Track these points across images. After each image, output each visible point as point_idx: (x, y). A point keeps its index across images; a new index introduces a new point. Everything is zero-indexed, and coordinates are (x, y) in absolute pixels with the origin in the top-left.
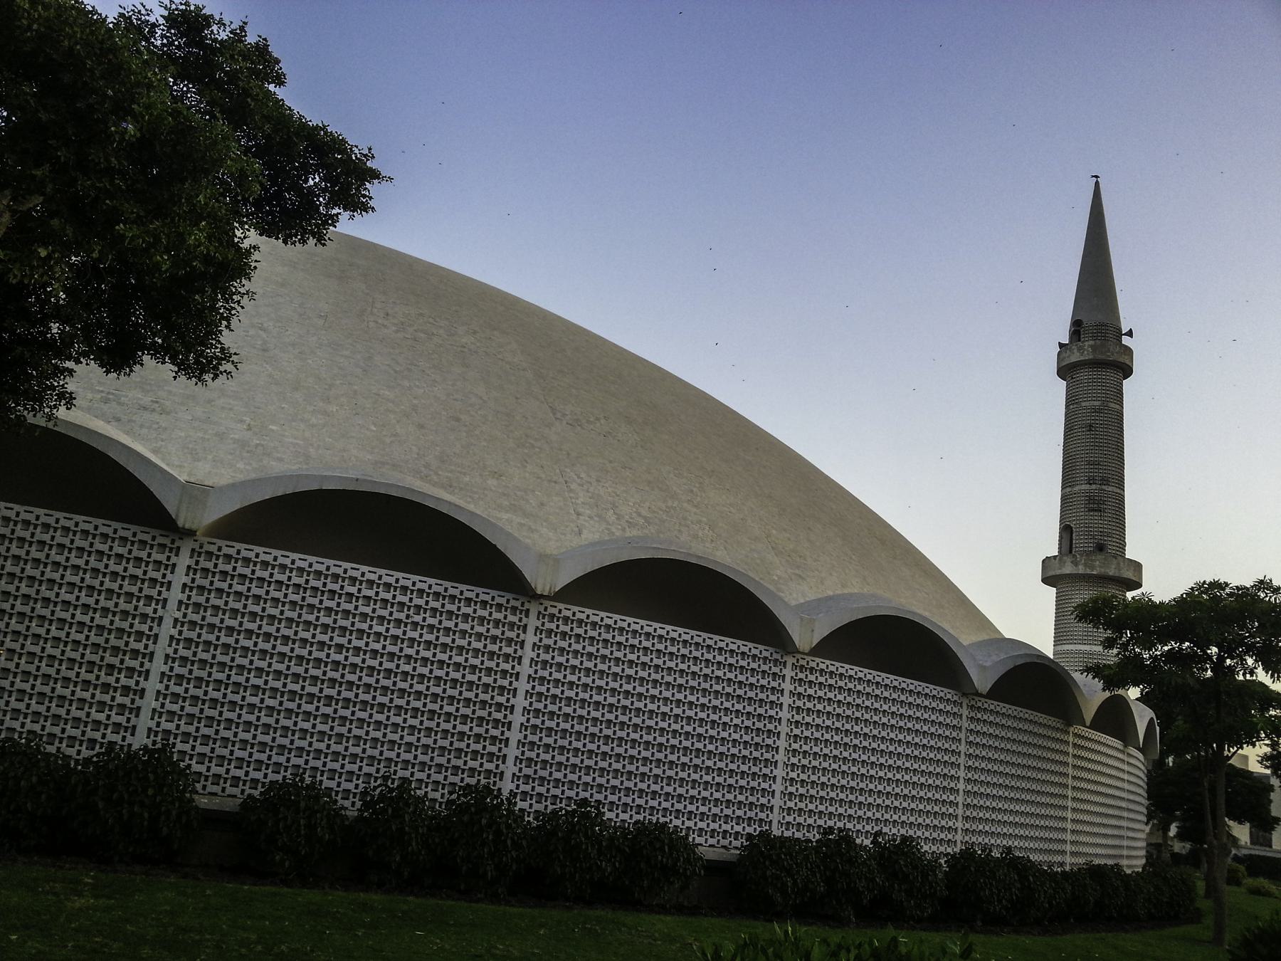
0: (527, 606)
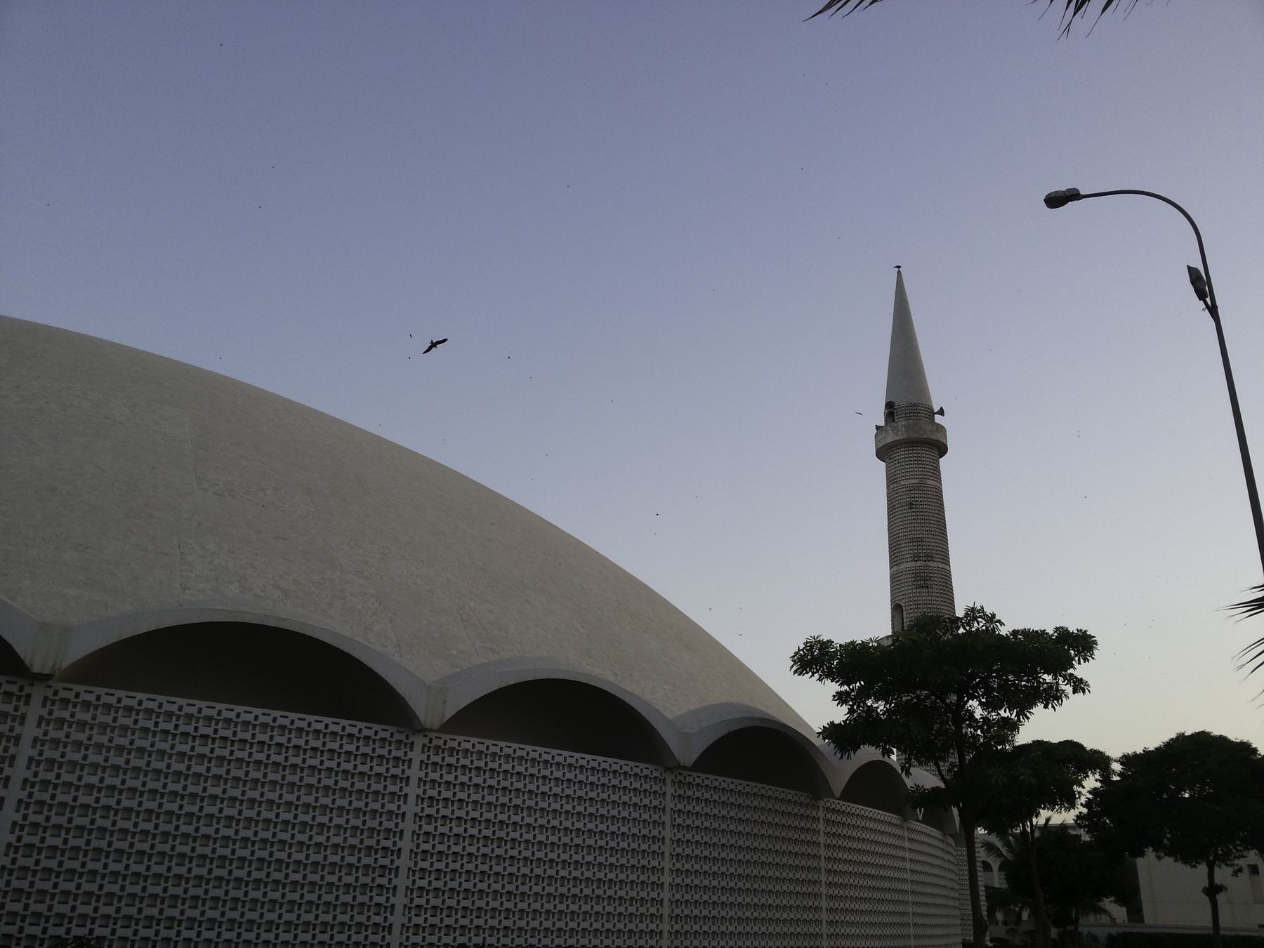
0: (27, 690)
